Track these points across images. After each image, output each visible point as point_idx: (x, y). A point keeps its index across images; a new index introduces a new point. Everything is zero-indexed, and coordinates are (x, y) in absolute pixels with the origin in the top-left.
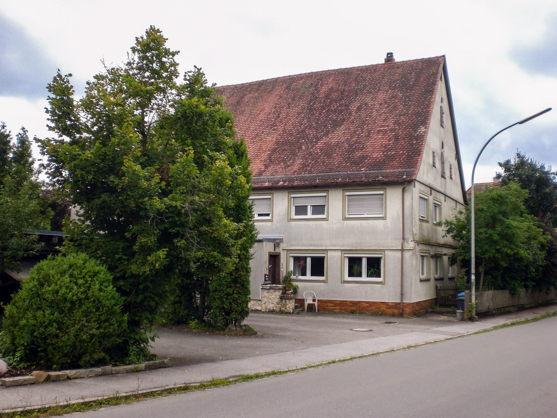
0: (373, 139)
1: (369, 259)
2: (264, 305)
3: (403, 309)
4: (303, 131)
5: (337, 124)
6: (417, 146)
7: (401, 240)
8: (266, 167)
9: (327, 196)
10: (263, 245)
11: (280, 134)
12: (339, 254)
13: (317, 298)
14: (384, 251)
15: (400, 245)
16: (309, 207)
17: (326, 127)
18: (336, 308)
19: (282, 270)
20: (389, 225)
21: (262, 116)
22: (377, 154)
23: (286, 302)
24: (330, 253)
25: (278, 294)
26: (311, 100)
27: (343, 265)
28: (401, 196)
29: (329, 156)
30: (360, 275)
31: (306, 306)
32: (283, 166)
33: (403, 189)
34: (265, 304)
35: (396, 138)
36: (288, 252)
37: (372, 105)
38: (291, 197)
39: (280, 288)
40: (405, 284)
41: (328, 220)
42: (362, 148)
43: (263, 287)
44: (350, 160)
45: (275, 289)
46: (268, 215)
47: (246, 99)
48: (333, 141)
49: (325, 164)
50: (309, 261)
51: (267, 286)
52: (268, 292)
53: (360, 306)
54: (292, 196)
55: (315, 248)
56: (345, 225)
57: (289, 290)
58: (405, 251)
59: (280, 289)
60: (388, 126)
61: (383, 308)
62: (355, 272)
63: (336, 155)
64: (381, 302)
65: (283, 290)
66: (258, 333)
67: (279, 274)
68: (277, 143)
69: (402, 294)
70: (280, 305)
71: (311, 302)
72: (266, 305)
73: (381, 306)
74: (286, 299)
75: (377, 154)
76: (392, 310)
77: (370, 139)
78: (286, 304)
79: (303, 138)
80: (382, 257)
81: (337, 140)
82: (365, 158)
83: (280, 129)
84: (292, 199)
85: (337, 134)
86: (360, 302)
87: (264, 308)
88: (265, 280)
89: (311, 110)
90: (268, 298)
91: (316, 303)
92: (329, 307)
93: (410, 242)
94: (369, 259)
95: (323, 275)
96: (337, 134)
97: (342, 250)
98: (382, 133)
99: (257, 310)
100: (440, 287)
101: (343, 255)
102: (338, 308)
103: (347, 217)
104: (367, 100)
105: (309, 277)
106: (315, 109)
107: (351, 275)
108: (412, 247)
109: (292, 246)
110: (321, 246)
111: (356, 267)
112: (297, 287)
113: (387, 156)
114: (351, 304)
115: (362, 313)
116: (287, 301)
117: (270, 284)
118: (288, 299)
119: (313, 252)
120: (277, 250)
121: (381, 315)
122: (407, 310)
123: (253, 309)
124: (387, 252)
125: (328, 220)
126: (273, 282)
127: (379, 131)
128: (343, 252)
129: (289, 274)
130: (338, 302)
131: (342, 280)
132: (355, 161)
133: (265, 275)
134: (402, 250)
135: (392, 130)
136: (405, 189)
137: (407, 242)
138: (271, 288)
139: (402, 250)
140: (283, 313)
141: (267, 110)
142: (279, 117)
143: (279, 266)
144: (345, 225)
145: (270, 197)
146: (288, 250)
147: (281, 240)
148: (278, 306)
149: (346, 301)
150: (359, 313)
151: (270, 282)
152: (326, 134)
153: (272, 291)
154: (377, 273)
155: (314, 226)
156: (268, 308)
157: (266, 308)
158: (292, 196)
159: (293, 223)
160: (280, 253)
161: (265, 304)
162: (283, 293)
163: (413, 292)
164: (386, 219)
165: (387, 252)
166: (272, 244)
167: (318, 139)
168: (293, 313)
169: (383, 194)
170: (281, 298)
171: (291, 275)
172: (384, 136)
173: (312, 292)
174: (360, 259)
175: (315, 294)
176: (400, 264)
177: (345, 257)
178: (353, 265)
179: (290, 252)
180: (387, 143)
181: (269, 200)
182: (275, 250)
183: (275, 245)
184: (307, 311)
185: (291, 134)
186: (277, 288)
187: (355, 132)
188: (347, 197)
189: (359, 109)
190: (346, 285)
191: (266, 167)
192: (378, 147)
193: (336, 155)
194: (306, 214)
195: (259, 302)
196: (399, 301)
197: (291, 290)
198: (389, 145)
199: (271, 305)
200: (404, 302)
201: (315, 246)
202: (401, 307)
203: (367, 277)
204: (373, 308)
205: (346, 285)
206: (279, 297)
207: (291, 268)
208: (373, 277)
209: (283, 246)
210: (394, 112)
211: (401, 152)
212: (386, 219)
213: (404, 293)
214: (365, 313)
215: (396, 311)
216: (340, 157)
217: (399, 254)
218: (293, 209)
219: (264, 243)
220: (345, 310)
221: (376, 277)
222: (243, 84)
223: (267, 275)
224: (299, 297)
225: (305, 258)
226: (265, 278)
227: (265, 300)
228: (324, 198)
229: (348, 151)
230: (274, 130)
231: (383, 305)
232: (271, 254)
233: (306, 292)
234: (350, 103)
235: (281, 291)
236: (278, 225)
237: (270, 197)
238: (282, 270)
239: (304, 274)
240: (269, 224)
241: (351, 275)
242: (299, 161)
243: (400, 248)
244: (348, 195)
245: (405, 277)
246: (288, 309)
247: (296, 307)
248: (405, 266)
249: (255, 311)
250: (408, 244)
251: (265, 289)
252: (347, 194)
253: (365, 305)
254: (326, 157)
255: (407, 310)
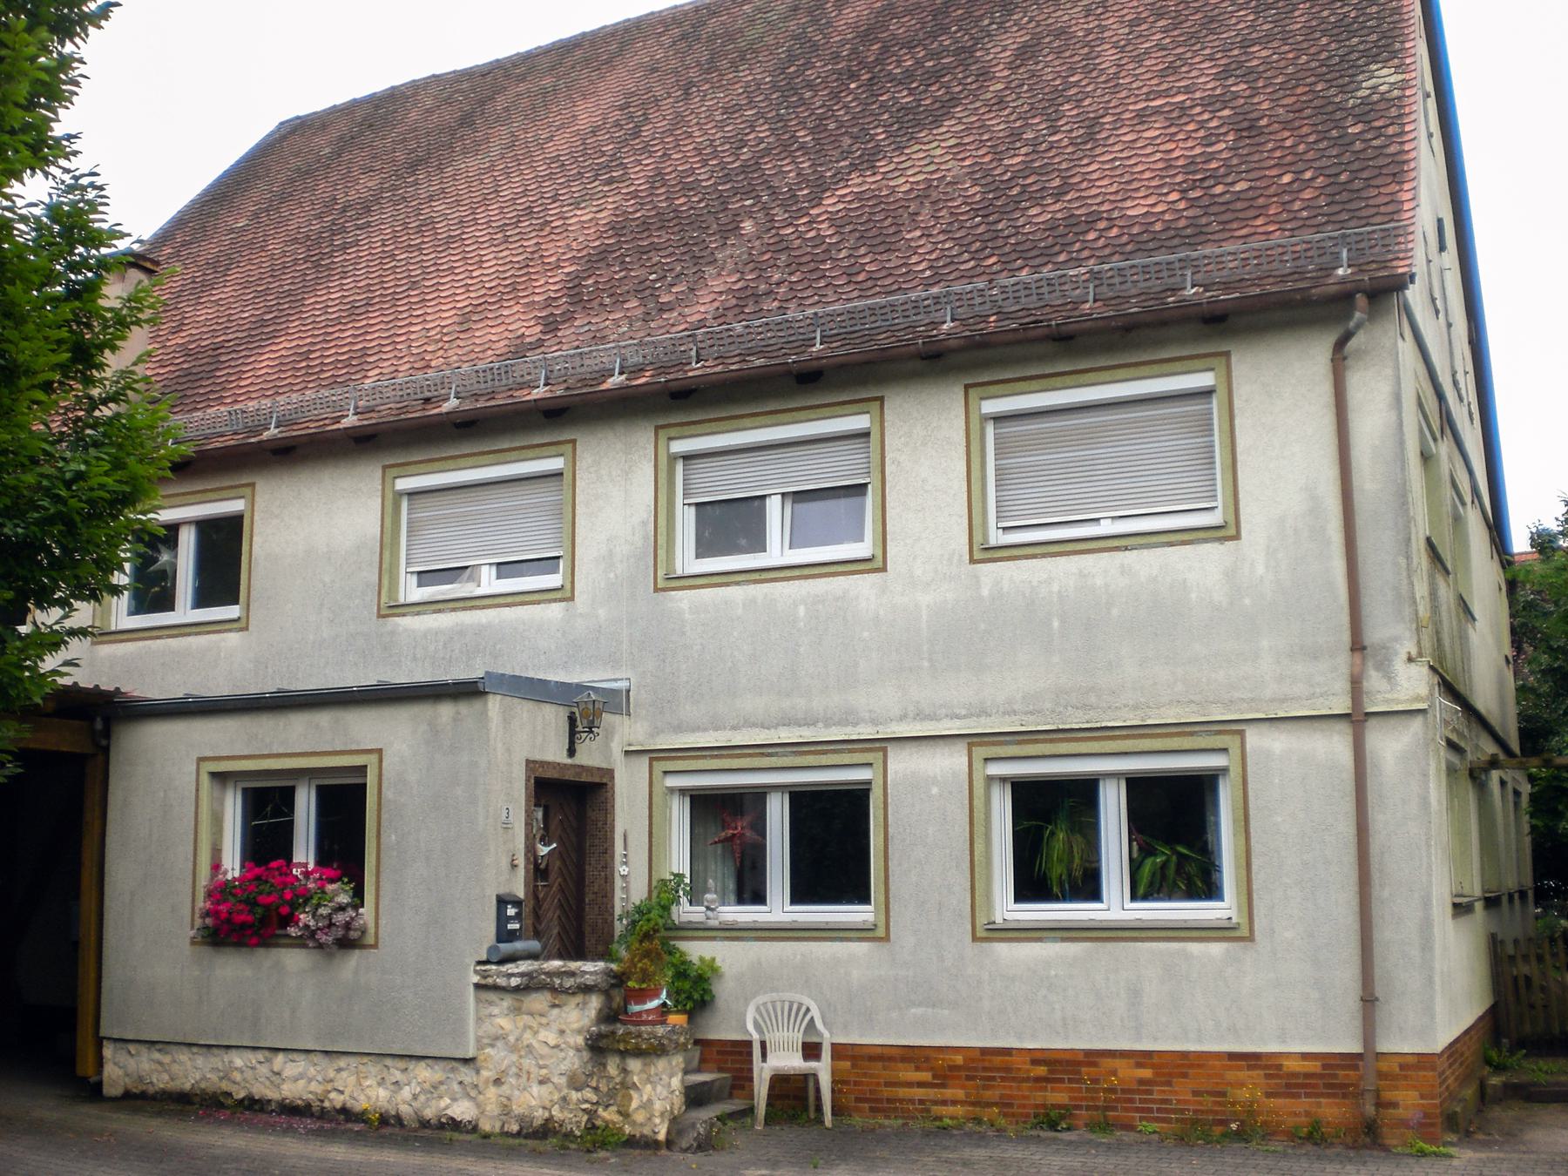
0: (1116, 148)
1: (1138, 786)
2: (492, 1092)
3: (1377, 1092)
4: (754, 165)
5: (910, 124)
6: (1375, 143)
7: (1343, 661)
8: (551, 326)
9: (875, 437)
10: (484, 713)
11: (634, 195)
12: (953, 761)
13: (827, 1038)
14: (1235, 728)
15: (1342, 685)
16: (774, 506)
17: (863, 136)
18: (949, 1093)
19: (624, 870)
20: (1260, 570)
21: (561, 145)
22: (1151, 201)
23: (625, 1071)
24: (901, 764)
25: (580, 1016)
26: (791, 59)
27: (979, 829)
28: (1326, 389)
29: (883, 243)
30: (1087, 887)
31: (761, 1090)
32: (639, 312)
33: (1340, 345)
34: (498, 1082)
35: (1247, 128)
36: (660, 767)
37: (1089, 32)
38: (673, 458)
39: (589, 980)
40: (1384, 934)
41: (884, 569)
42: (1058, 195)
43: (485, 975)
44: (1000, 242)
45: (557, 990)
46: (547, 564)
47: (501, 102)
48: (902, 185)
49: (861, 278)
50: (778, 814)
51: (510, 968)
52: (517, 1011)
53: (1095, 1081)
54: (679, 447)
55: (807, 734)
56: (985, 592)
57: (643, 995)
58: (1372, 723)
59: (586, 989)
60: (1187, 90)
61: (1248, 1090)
62: (1057, 871)
63: (918, 233)
64: (1233, 1056)
65: (606, 993)
66: (1428, 533)
67: (607, 895)
68: (616, 228)
69: (1368, 1001)
70: (589, 1094)
71: (793, 1062)
72: (505, 1089)
73: (1231, 1076)
74: (624, 1054)
75: (1151, 201)
76: (1303, 1104)
77: (1098, 151)
78: (627, 1086)
79: (750, 192)
80: (1224, 770)
81: (921, 177)
82: (1083, 227)
83: (639, 178)
84: (679, 467)
85: (921, 155)
86: (1093, 1057)
87: (492, 1108)
88: (504, 935)
89: (789, 88)
90: (514, 1049)
91: (823, 1069)
92: (903, 1092)
93: (1399, 666)
94: (1138, 786)
95: (864, 899)
96: (921, 155)
97: (974, 740)
98: (1161, 118)
99: (455, 1125)
100: (1516, 942)
101: (977, 765)
102: (960, 1094)
103: (993, 542)
104: (1066, 18)
105: (779, 908)
106: (810, 85)
107: (1030, 886)
108: (1418, 699)
109: (679, 729)
110: (842, 723)
111: (1059, 839)
112: (715, 970)
113: (1209, 205)
114: (1042, 1070)
115: (1106, 1126)
116: (634, 1065)
117: (533, 956)
118: (638, 1053)
119: (799, 761)
120: (589, 755)
121: (1241, 1136)
122: (1409, 1101)
123: (429, 1113)
124: (1255, 739)
125: (884, 569)
126: (575, 948)
127: (1141, 116)
128: (980, 752)
129: (664, 893)
130: (959, 1059)
131: (981, 920)
132: (1028, 245)
133: (502, 902)
134: (1357, 719)
135: (1209, 103)
136: (1352, 344)
137: (1384, 666)
138: (530, 985)
139: (1357, 719)
140: (603, 1145)
141: (584, 122)
142: (636, 134)
143: (608, 851)
144: (985, 592)
145: (555, 464)
146: (655, 755)
147: (616, 701)
148: (575, 1096)
149: (1007, 1052)
150: (1092, 1126)
151: (534, 945)
152: (868, 162)
153: (539, 1001)
154: (1191, 869)
155: (802, 610)
156: (517, 1110)
157: (506, 1110)
158: (679, 447)
159: (683, 600)
160: (610, 773)
161: (498, 1082)
162: (610, 1016)
163: (1437, 979)
164: (1237, 537)
165: (1255, 739)
166: (553, 718)
167: (820, 188)
168: (669, 1143)
169: (1207, 393)
170: (598, 1047)
171: (677, 901)
172: (1173, 130)
173: (798, 997)
174: (1084, 792)
175: (815, 1013)
176: (1349, 806)
177: (990, 779)
178: (1040, 829)
179: (670, 766)
180: (1198, 150)
181: (551, 485)
182: (572, 752)
183: (572, 720)
184: (769, 1120)
185: (687, 188)
186: (569, 982)
187: (1015, 135)
188: (990, 429)
189: (1025, 53)
190: (1005, 951)
191: (551, 326)
192: (1147, 175)
193: (918, 233)
194: (759, 545)
195: (466, 1074)
196: (1355, 1047)
197: (657, 995)
198: (1211, 157)
199: (535, 1089)
200: (1385, 1046)
201: (810, 722)
202: (1370, 1083)
203: (1134, 898)
204: (1181, 1092)
205: (1003, 950)
206: (580, 1040)
207: (679, 860)
208: (1170, 898)
209: (624, 732)
210: (1211, 37)
211: (1286, 179)
212: (1237, 537)
213: (1379, 992)
214: (1129, 1127)
215: (1331, 1111)
216: (941, 238)
217: (1335, 746)
218: (686, 521)
219: (494, 704)
220: (1004, 1104)
221: (1192, 894)
222: (498, 61)
223: (517, 903)
224: (721, 1030)
225: (758, 796)
226: (502, 919)
227: (497, 1057)
228: (857, 444)
229: (983, 210)
230: (610, 182)
231: (1243, 1075)
232: (541, 773)
233: (760, 999)
234: (977, 41)
235: (595, 1002)
236: (602, 612)
237: (555, 464)
238: (624, 870)
239: (754, 894)
240: (555, 611)
241: (1030, 886)
242: (719, 284)
243: (1342, 705)
244: (999, 419)
245: (1380, 892)
246: (640, 1117)
247: (695, 1097)
248: (1380, 820)
249: (441, 1126)
250: (1389, 677)
251: (496, 988)
252: (991, 407)
253: (1130, 1073)
254: (863, 251)
255: (1409, 1101)
